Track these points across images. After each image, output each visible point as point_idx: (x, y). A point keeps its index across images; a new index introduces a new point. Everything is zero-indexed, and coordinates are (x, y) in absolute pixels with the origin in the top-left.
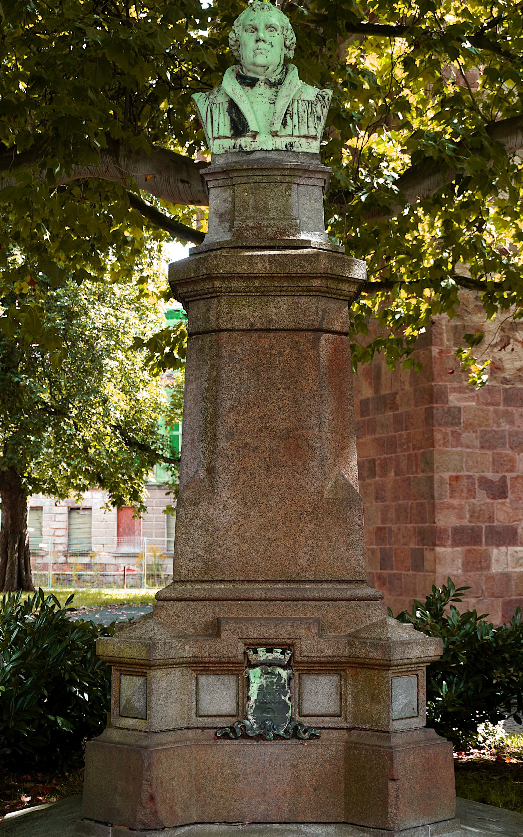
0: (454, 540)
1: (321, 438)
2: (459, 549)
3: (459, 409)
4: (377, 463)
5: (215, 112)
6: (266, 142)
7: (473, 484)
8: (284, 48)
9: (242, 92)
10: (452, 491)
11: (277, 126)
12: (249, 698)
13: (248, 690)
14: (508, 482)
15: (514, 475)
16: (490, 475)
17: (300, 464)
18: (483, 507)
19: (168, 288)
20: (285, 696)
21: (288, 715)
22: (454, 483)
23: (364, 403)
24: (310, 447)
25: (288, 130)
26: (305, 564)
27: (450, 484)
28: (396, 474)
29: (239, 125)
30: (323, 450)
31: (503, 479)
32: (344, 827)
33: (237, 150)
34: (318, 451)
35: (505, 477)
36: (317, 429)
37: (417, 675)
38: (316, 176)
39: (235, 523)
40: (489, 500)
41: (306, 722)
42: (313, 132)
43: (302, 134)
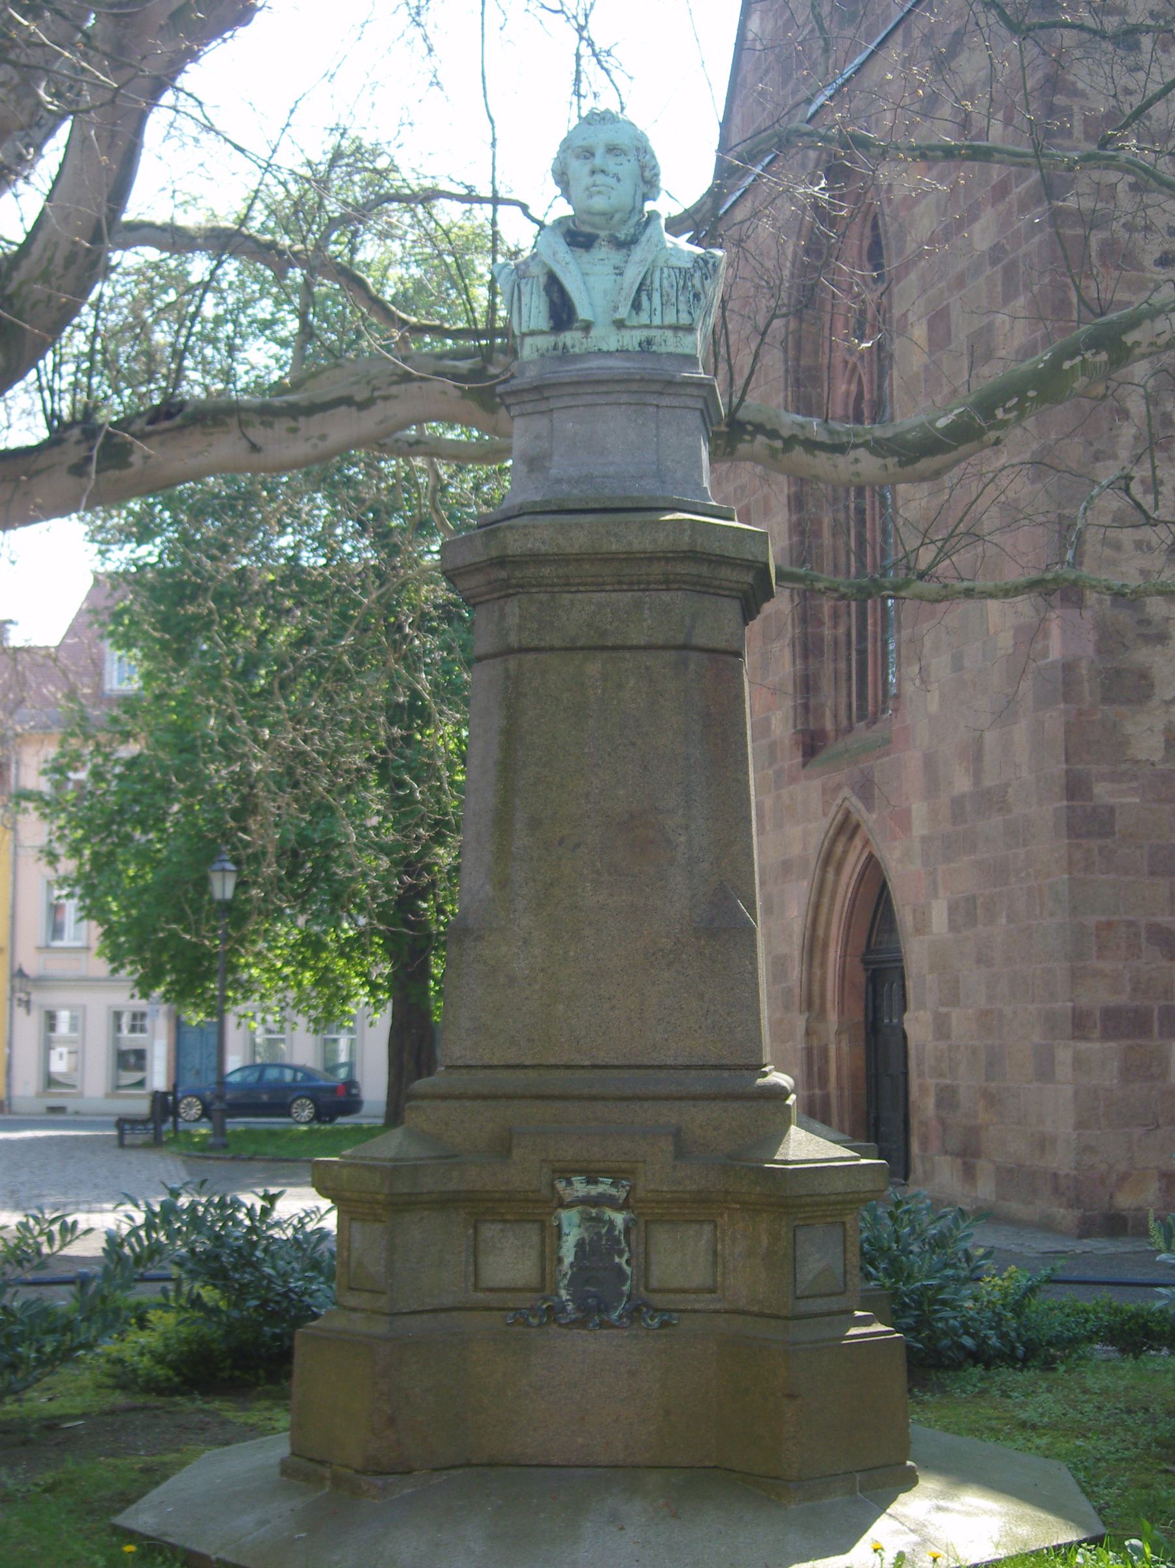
1: (687, 827)
2: (1112, 1044)
3: (1111, 810)
4: (978, 902)
5: (526, 289)
6: (607, 339)
8: (641, 184)
9: (569, 258)
11: (624, 312)
12: (560, 1260)
13: (560, 1247)
19: (81, 519)
20: (621, 1256)
21: (626, 1288)
23: (958, 803)
25: (644, 318)
27: (1098, 936)
28: (1010, 920)
33: (559, 352)
36: (680, 812)
37: (843, 1223)
38: (689, 390)
39: (542, 970)
41: (657, 1300)
43: (666, 322)
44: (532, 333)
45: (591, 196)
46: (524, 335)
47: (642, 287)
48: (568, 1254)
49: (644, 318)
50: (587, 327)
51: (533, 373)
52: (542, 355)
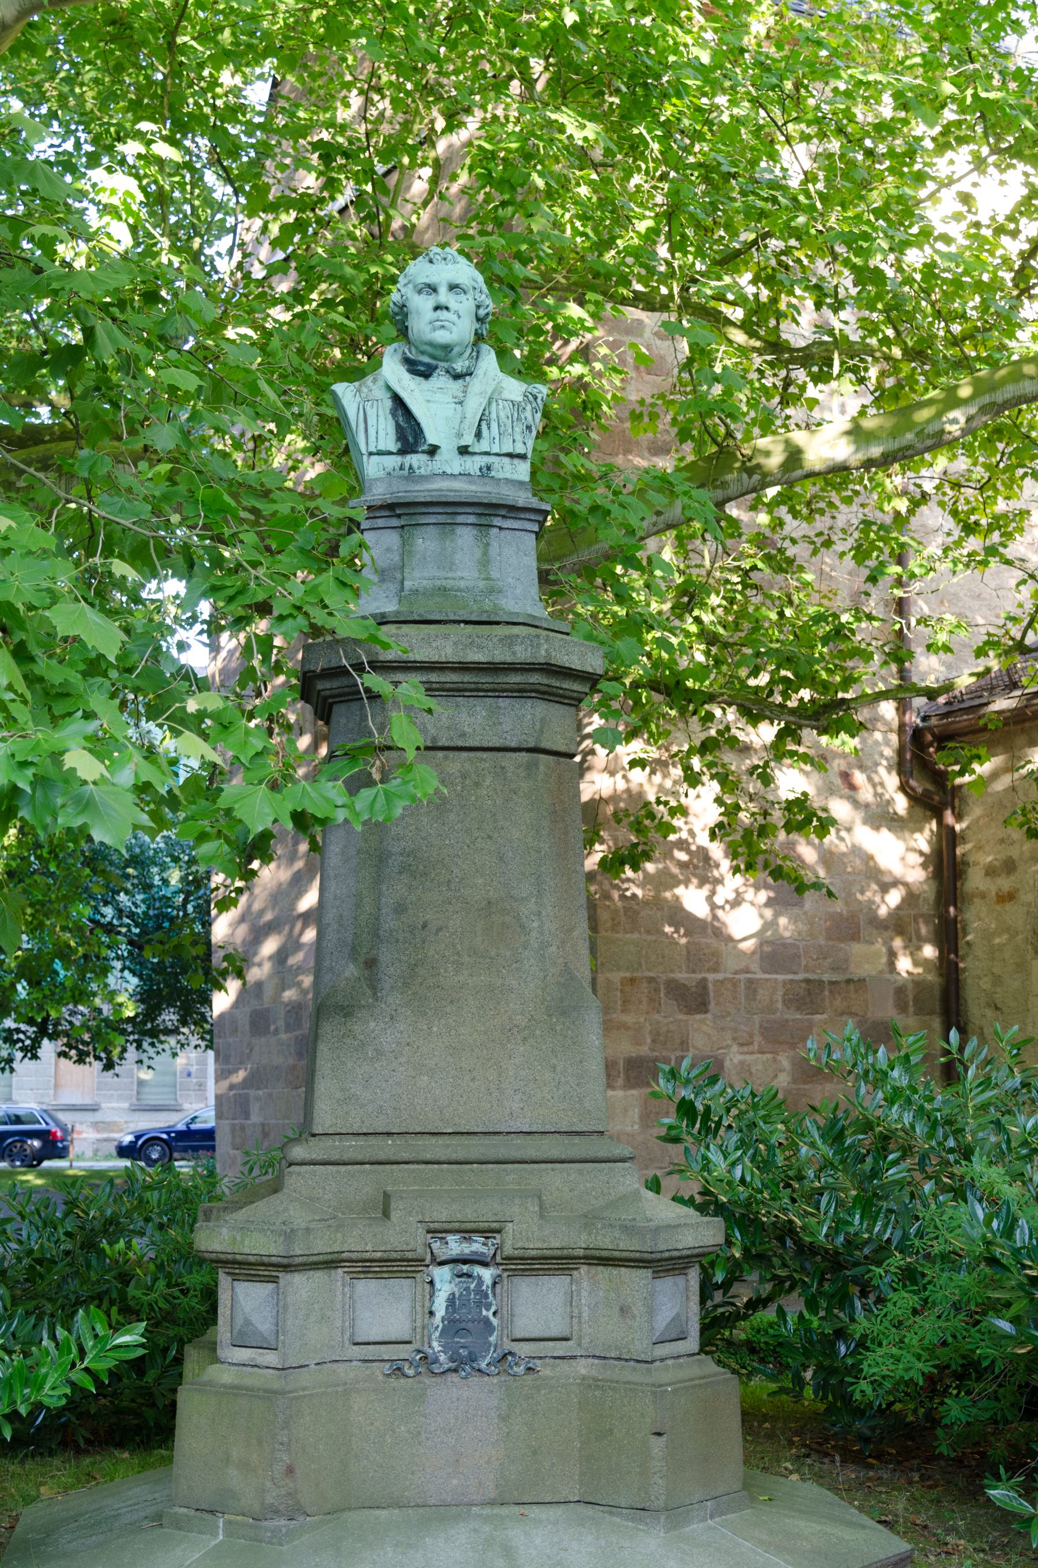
0: (628, 1078)
1: (539, 914)
2: (634, 1092)
7: (657, 990)
10: (625, 1002)
14: (710, 986)
15: (720, 976)
16: (681, 976)
17: (508, 953)
18: (672, 1027)
21: (492, 1339)
22: (627, 989)
24: (522, 927)
26: (516, 1106)
29: (410, 435)
30: (542, 933)
31: (703, 983)
32: (582, 1509)
33: (406, 472)
34: (534, 934)
35: (705, 980)
38: (528, 516)
40: (681, 1017)
42: (520, 449)
44: (380, 453)
46: (371, 454)
48: (440, 1308)
49: (484, 446)
50: (433, 451)
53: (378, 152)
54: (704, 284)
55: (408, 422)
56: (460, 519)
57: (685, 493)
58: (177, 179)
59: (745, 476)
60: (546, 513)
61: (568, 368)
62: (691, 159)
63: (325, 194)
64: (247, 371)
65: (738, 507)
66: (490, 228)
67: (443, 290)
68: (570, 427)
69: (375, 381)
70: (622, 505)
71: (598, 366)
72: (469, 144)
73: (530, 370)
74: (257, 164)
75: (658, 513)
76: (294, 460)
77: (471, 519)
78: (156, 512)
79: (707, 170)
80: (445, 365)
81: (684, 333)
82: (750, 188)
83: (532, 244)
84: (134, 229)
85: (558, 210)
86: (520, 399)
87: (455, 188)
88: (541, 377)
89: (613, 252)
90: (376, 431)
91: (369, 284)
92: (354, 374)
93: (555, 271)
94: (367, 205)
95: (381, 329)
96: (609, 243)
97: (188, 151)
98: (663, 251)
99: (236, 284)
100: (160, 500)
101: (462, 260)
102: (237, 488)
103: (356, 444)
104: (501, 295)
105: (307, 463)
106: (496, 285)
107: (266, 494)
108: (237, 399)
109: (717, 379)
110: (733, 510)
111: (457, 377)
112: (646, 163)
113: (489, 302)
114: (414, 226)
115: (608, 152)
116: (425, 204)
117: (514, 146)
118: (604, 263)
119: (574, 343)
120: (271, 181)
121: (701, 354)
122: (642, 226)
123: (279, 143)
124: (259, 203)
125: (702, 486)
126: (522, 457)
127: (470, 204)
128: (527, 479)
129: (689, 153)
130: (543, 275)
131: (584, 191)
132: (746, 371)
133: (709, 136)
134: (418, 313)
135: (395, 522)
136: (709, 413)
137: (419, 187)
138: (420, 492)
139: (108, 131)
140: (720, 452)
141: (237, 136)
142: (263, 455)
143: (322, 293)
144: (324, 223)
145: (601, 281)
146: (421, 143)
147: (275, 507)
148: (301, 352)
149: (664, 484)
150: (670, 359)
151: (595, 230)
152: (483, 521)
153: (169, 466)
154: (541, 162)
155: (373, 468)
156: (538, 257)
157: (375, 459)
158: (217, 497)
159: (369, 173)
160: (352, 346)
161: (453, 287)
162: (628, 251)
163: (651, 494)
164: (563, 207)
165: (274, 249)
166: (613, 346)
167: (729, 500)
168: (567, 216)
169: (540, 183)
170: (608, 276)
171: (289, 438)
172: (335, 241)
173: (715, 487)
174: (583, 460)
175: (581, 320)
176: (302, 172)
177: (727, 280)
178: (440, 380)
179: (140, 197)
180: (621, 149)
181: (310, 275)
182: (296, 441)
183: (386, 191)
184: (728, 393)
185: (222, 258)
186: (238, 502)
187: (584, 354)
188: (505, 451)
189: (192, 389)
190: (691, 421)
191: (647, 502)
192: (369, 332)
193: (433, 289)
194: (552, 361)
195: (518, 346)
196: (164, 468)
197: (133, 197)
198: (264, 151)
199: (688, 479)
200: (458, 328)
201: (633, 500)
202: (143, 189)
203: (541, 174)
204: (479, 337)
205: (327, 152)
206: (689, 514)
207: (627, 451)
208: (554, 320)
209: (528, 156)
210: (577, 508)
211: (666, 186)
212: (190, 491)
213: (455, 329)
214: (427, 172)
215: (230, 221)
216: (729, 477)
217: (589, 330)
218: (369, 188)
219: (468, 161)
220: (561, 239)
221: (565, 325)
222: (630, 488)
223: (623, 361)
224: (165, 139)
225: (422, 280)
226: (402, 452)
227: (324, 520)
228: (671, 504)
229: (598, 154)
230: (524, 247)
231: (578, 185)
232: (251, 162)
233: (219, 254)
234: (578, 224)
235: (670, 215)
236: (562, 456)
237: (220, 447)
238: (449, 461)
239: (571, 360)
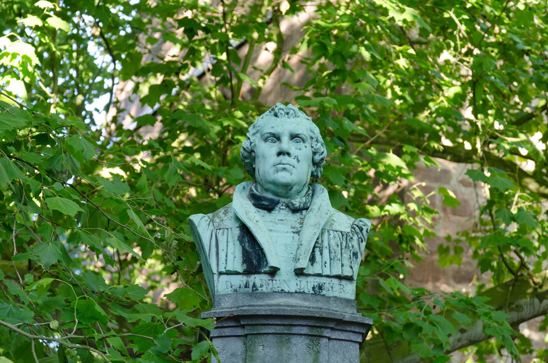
5: (222, 240)
29: (254, 257)
33: (250, 290)
38: (353, 329)
42: (347, 272)
44: (228, 273)
45: (277, 171)
46: (221, 273)
47: (317, 245)
49: (317, 269)
50: (273, 272)
51: (228, 304)
52: (236, 290)
53: (233, 29)
54: (503, 140)
55: (253, 247)
56: (295, 330)
57: (486, 314)
58: (66, 47)
59: (536, 301)
60: (369, 327)
61: (387, 207)
62: (492, 39)
63: (188, 62)
64: (119, 202)
65: (530, 328)
66: (323, 92)
67: (285, 139)
68: (388, 257)
69: (226, 213)
70: (432, 323)
71: (413, 206)
72: (308, 23)
73: (355, 208)
74: (132, 36)
75: (463, 331)
76: (153, 279)
77: (305, 330)
78: (38, 317)
79: (505, 49)
80: (285, 200)
81: (486, 180)
82: (541, 62)
83: (359, 104)
84: (29, 87)
85: (382, 79)
86: (349, 230)
87: (295, 59)
88: (365, 213)
89: (426, 113)
90: (227, 255)
91: (221, 135)
92: (209, 208)
93: (377, 127)
94: (222, 71)
95: (232, 171)
96: (423, 105)
97: (77, 26)
98: (468, 113)
99: (110, 134)
100: (42, 308)
101: (301, 114)
102: (107, 300)
103: (209, 266)
104: (332, 145)
105: (164, 283)
106: (328, 138)
107: (130, 306)
108: (109, 226)
109: (513, 219)
110: (525, 331)
111: (295, 211)
112: (455, 40)
113: (323, 149)
114: (260, 89)
115: (423, 32)
116: (269, 73)
117: (345, 25)
118: (419, 122)
119: (392, 188)
120: (143, 51)
121: (499, 199)
122: (451, 91)
123: (150, 22)
124: (133, 68)
125: (499, 308)
126: (349, 279)
127: (308, 71)
128: (353, 297)
129: (490, 34)
130: (368, 130)
131: (402, 63)
132: (537, 213)
133: (506, 21)
134: (264, 157)
135: (240, 332)
136: (506, 248)
137: (265, 55)
138: (262, 306)
139: (11, 8)
140: (516, 280)
141: (116, 15)
142: (127, 277)
143: (182, 142)
144: (184, 86)
145: (415, 137)
146: (268, 23)
147: (137, 316)
148: (163, 189)
149: (468, 306)
150: (472, 203)
151: (412, 95)
152: (315, 332)
153: (51, 280)
154: (368, 39)
155: (222, 285)
156: (364, 115)
157: (224, 278)
158: (89, 307)
159: (224, 44)
160: (207, 186)
161: (294, 137)
162: (440, 112)
163: (457, 315)
164: (385, 75)
165: (143, 105)
166: (426, 190)
167: (523, 320)
168: (389, 83)
169: (366, 55)
170: (421, 133)
171: (150, 261)
172: (193, 101)
173: (511, 310)
174: (399, 284)
175: (399, 168)
176: (168, 44)
177: (522, 137)
178: (281, 213)
179: (36, 61)
180: (434, 30)
181: (172, 126)
182: (154, 264)
183: (237, 60)
184: (522, 230)
185: (99, 113)
186: (107, 312)
187: (401, 196)
188: (334, 273)
189: (73, 214)
190: (490, 254)
191: (454, 322)
192: (220, 174)
193: (277, 138)
194: (372, 203)
195: (346, 188)
196: (46, 281)
197: (30, 60)
198: (138, 27)
199: (488, 303)
200: (298, 171)
201: (442, 319)
202: (39, 55)
203: (367, 48)
204: (314, 179)
205: (190, 27)
206: (488, 332)
207: (436, 279)
208: (375, 166)
209: (357, 34)
210: (393, 325)
211: (471, 60)
212: (67, 301)
213: (294, 171)
214: (272, 46)
215: (108, 83)
216: (522, 302)
217: (405, 176)
218: (224, 57)
219: (307, 38)
220: (384, 101)
221: (385, 172)
222: (438, 310)
223: (433, 204)
224: (58, 14)
225: (268, 130)
226: (247, 273)
227: (179, 329)
228: (473, 323)
229: (414, 34)
230: (352, 106)
231: (398, 57)
232: (128, 36)
233: (97, 110)
234: (397, 89)
235: (474, 84)
236: (381, 281)
237: (92, 268)
238: (286, 281)
239: (390, 201)
